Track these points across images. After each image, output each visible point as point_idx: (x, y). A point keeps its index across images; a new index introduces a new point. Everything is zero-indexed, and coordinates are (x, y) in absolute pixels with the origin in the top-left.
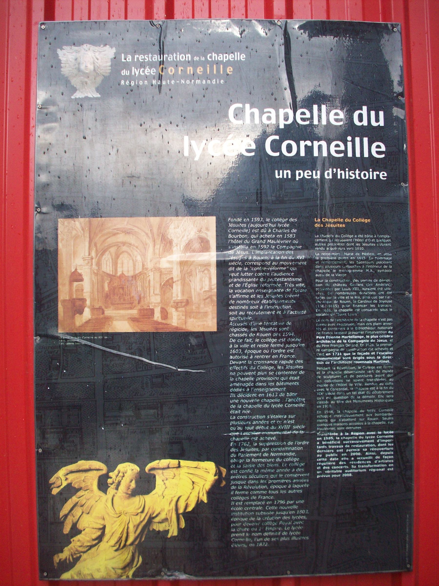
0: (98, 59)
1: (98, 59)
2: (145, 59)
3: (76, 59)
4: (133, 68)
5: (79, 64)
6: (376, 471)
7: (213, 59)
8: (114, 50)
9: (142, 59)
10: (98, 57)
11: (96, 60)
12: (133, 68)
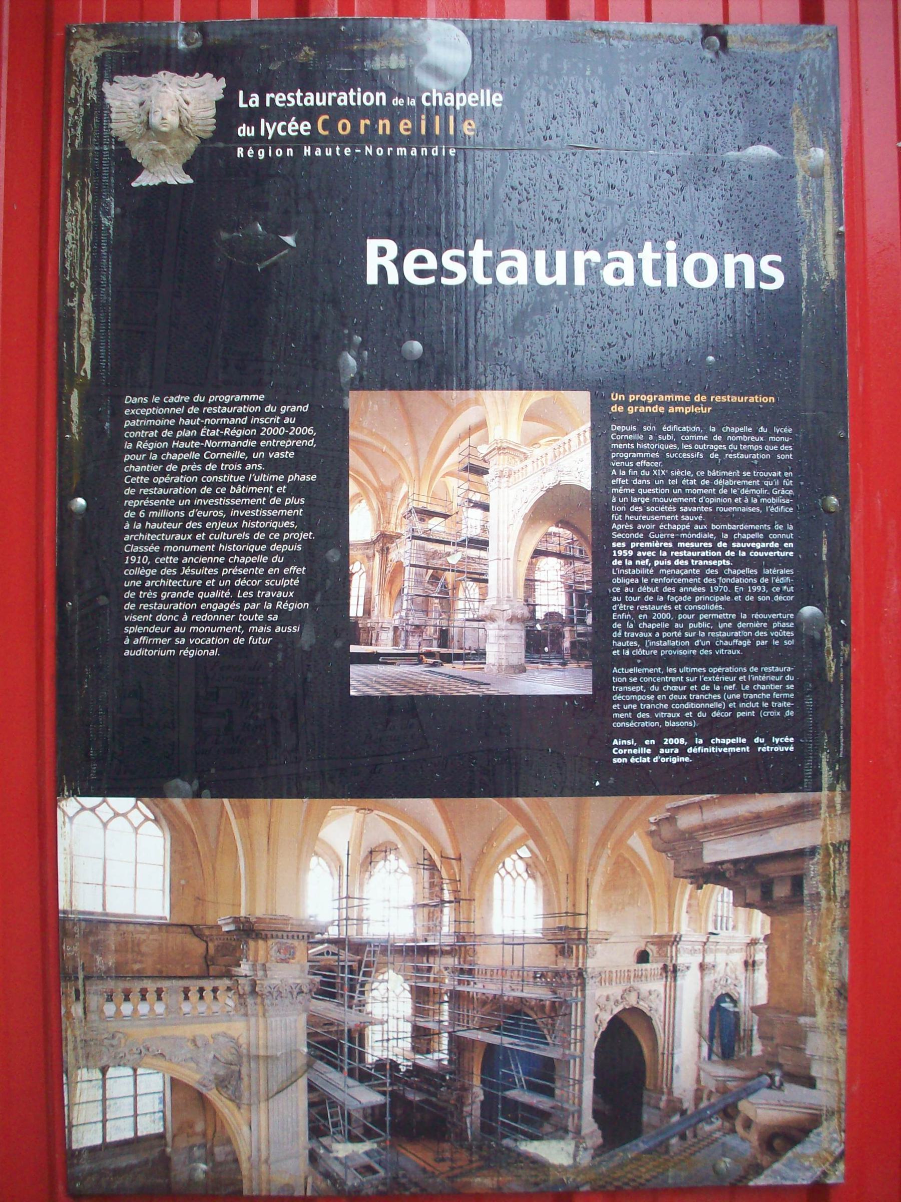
0: (187, 103)
1: (187, 103)
2: (288, 101)
3: (142, 104)
6: (196, 657)
7: (434, 104)
10: (188, 98)
11: (185, 106)
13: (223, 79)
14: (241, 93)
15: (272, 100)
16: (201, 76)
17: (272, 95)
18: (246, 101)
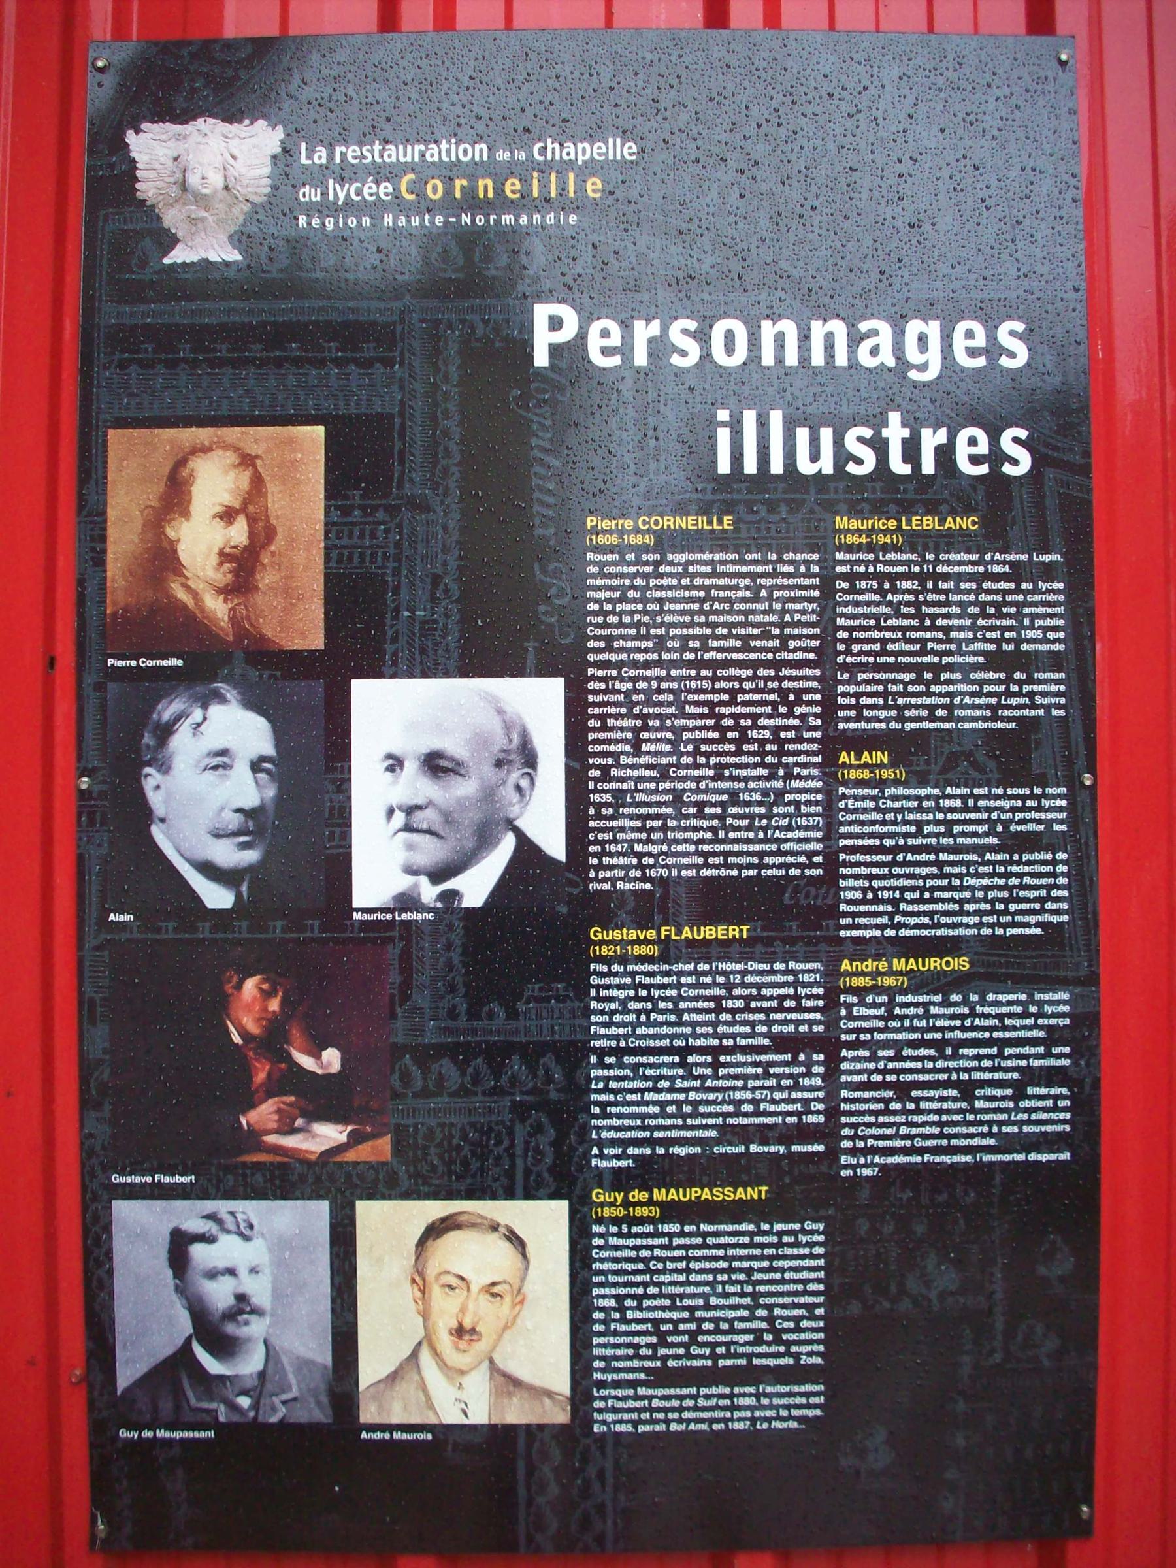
2: (363, 157)
8: (280, 133)
10: (236, 153)
13: (280, 128)
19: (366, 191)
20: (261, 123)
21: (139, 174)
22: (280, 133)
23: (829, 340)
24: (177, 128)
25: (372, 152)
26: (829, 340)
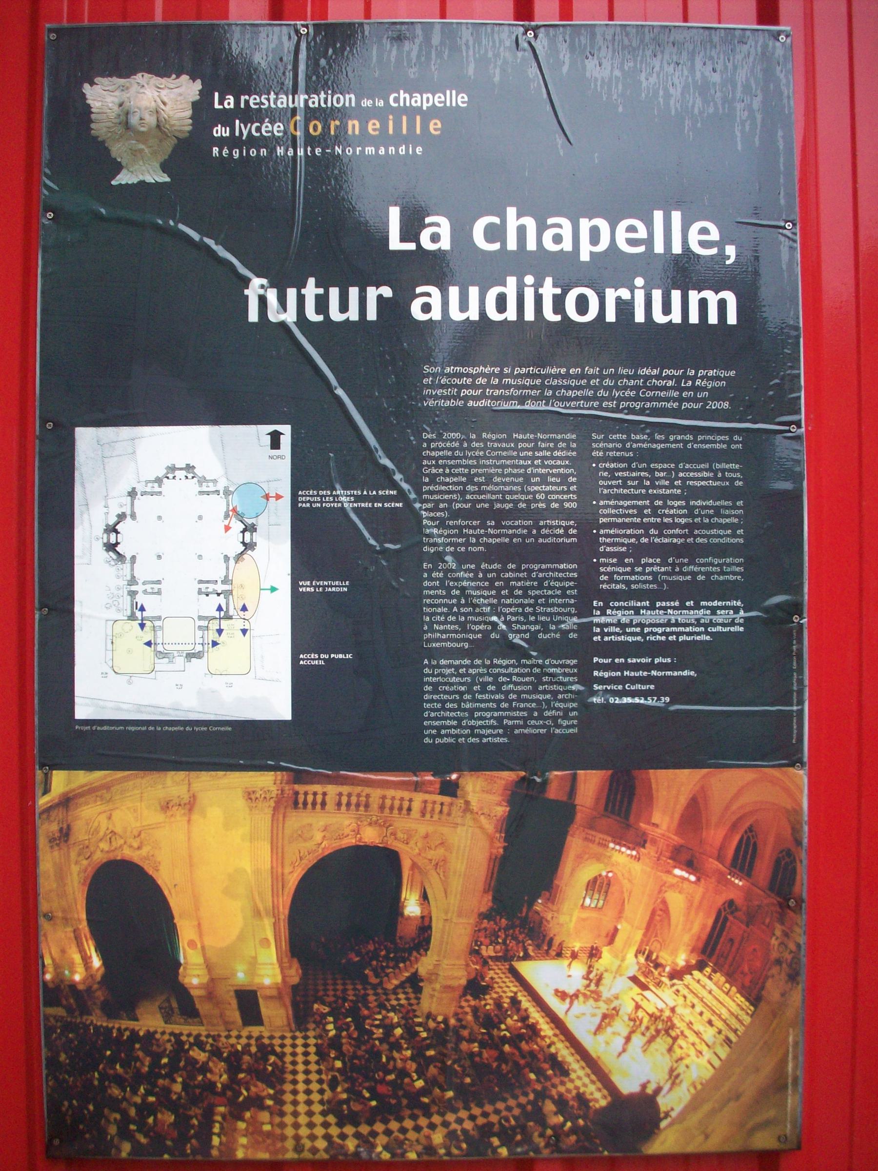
0: (164, 104)
1: (164, 104)
3: (121, 105)
4: (237, 122)
5: (127, 113)
7: (402, 104)
8: (198, 85)
9: (255, 104)
10: (166, 99)
11: (162, 106)
12: (237, 122)
13: (199, 82)
14: (217, 94)
15: (247, 102)
16: (178, 77)
17: (247, 97)
18: (221, 102)
19: (263, 130)
20: (185, 78)
21: (93, 116)
22: (198, 85)
23: (344, 307)
24: (122, 81)
25: (268, 100)
26: (344, 307)
